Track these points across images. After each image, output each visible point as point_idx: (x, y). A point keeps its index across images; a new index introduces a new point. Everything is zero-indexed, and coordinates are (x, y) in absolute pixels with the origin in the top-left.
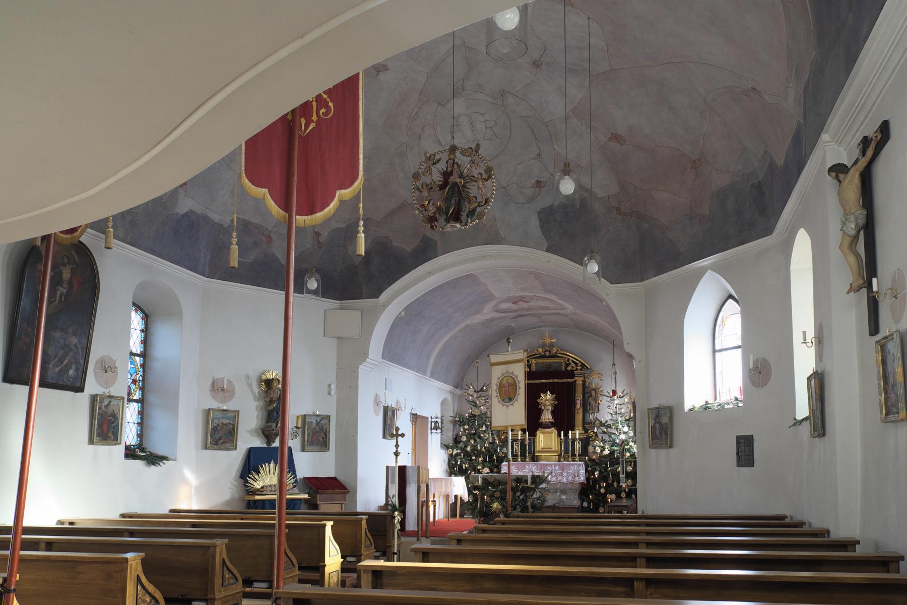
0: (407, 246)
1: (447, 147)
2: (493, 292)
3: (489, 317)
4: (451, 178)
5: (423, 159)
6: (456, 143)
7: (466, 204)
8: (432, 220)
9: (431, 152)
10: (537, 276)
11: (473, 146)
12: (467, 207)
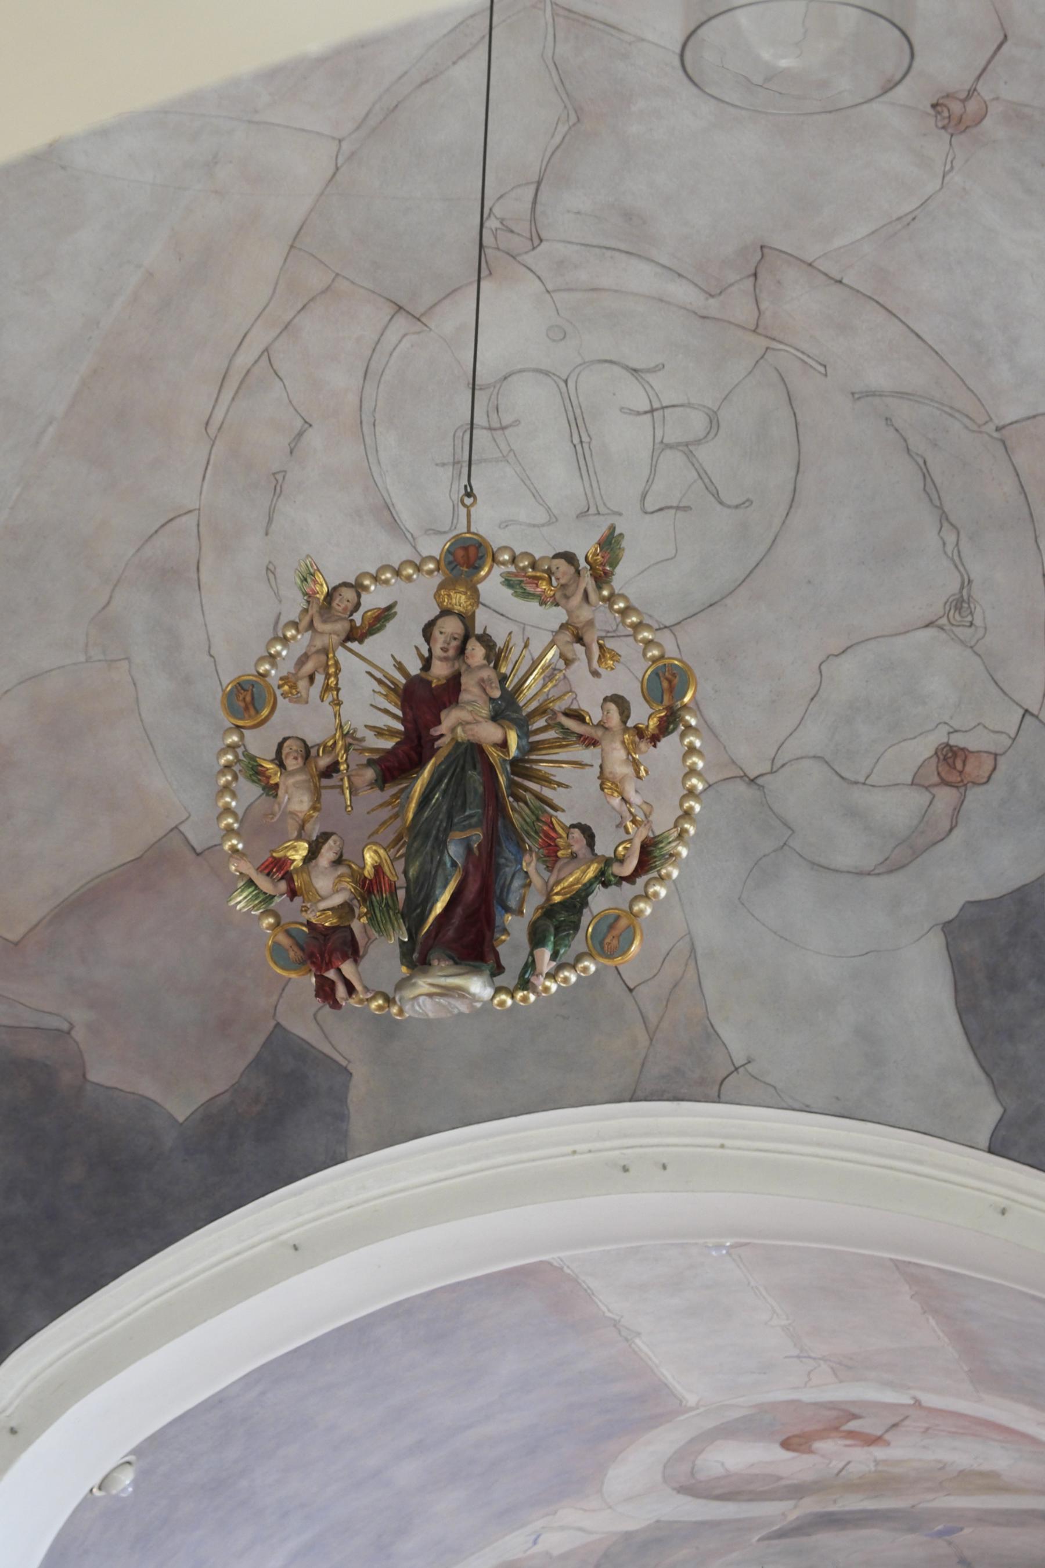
0: (166, 1082)
1: (434, 547)
2: (668, 1374)
3: (636, 1519)
4: (450, 718)
5: (293, 606)
6: (487, 523)
7: (531, 865)
8: (326, 949)
9: (335, 570)
10: (934, 1290)
11: (584, 546)
12: (532, 885)
